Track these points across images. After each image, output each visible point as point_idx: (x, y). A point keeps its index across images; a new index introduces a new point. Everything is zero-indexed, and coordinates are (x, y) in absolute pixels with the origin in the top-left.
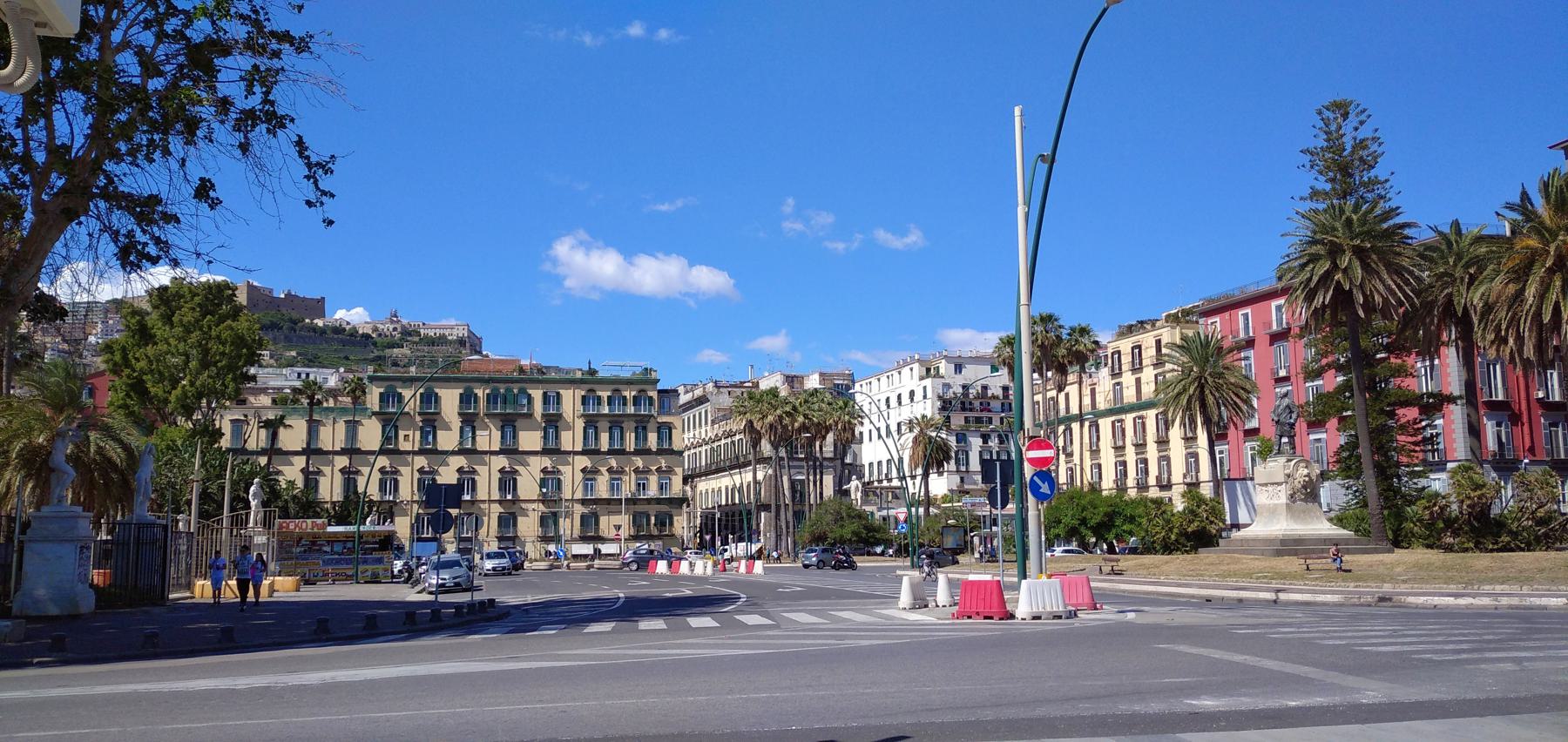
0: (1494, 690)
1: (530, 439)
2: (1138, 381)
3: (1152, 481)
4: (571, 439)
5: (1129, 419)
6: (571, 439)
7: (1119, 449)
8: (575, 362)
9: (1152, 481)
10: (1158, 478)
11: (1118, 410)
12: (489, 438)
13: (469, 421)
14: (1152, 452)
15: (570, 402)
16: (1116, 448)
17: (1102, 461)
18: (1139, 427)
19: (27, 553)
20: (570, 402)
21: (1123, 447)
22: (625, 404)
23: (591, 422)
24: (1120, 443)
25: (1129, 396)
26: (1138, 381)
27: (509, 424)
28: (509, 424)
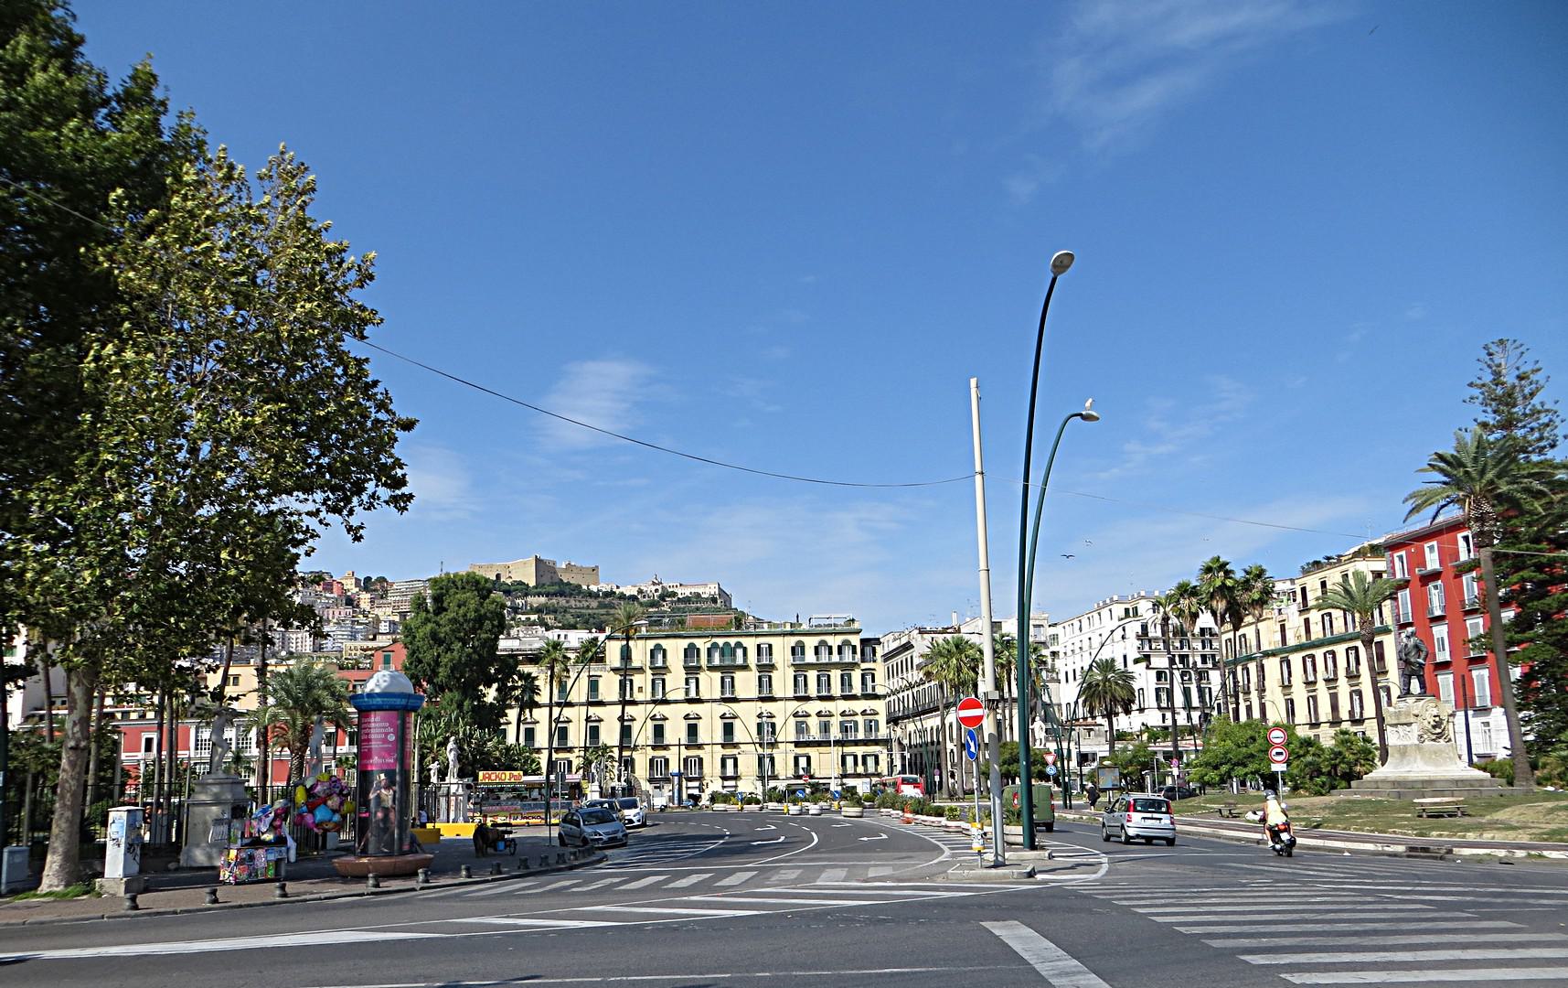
0: (689, 844)
1: (746, 683)
2: (1307, 621)
3: (1344, 715)
4: (783, 682)
5: (1319, 653)
6: (783, 682)
7: (1286, 687)
8: (784, 618)
9: (1344, 715)
10: (1351, 713)
11: (1283, 653)
12: (710, 684)
13: (692, 671)
14: (1343, 687)
15: (782, 647)
16: (1307, 683)
17: (1294, 696)
18: (1352, 658)
19: (44, 695)
20: (782, 647)
21: (1314, 683)
22: (830, 653)
23: (801, 668)
24: (1311, 678)
25: (1317, 633)
26: (1307, 621)
27: (728, 670)
28: (728, 670)
